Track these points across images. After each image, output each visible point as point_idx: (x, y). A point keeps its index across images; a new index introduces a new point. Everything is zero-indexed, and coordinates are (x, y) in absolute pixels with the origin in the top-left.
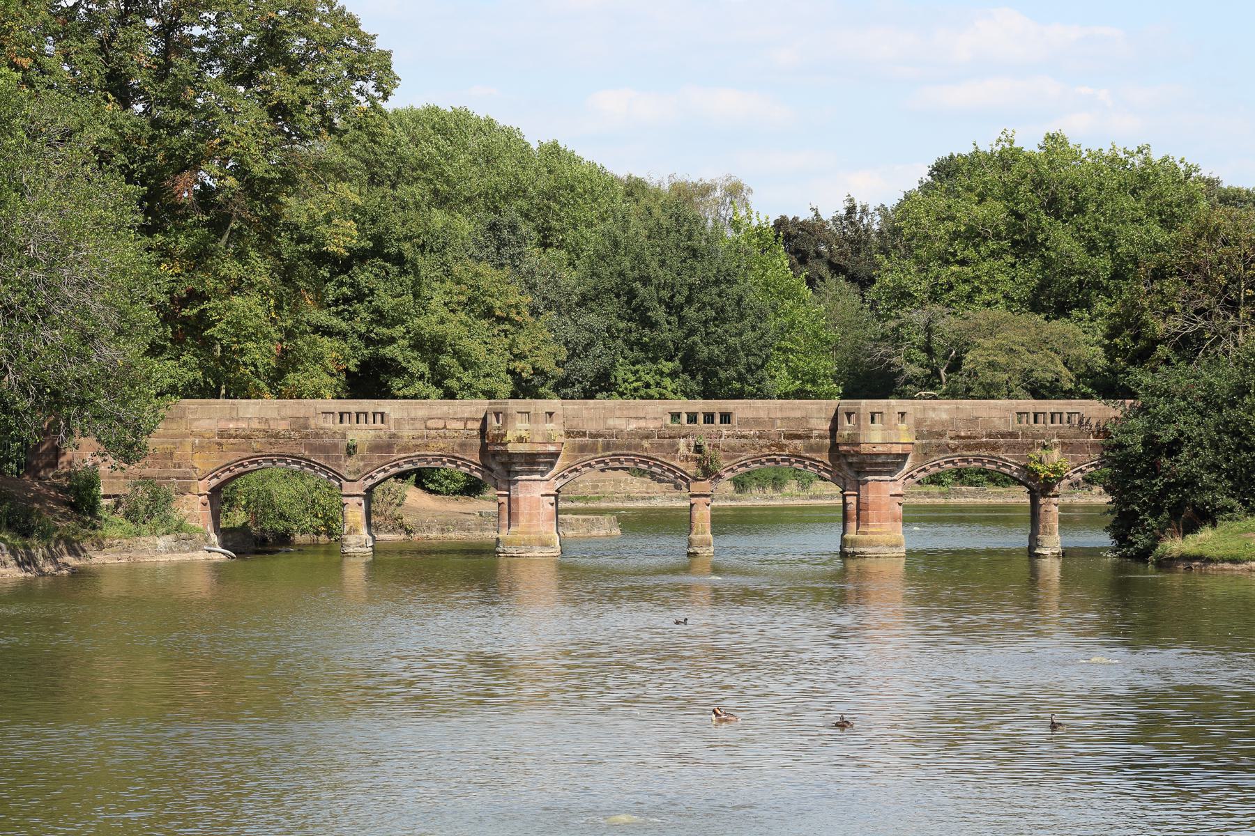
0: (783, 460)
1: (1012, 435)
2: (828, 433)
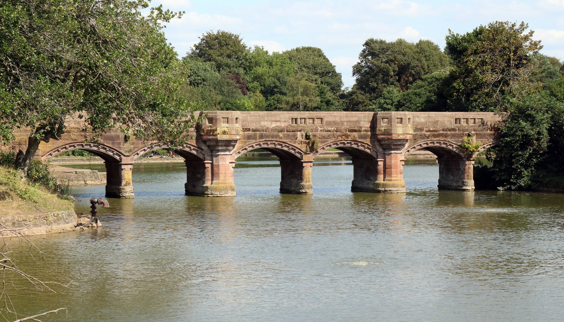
0: (348, 143)
1: (454, 130)
2: (369, 129)
